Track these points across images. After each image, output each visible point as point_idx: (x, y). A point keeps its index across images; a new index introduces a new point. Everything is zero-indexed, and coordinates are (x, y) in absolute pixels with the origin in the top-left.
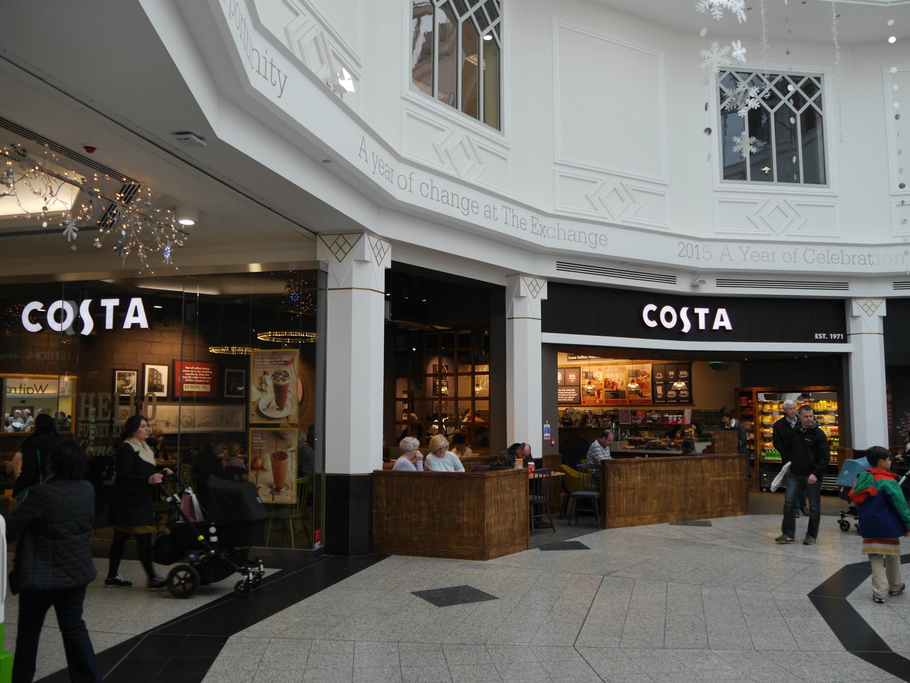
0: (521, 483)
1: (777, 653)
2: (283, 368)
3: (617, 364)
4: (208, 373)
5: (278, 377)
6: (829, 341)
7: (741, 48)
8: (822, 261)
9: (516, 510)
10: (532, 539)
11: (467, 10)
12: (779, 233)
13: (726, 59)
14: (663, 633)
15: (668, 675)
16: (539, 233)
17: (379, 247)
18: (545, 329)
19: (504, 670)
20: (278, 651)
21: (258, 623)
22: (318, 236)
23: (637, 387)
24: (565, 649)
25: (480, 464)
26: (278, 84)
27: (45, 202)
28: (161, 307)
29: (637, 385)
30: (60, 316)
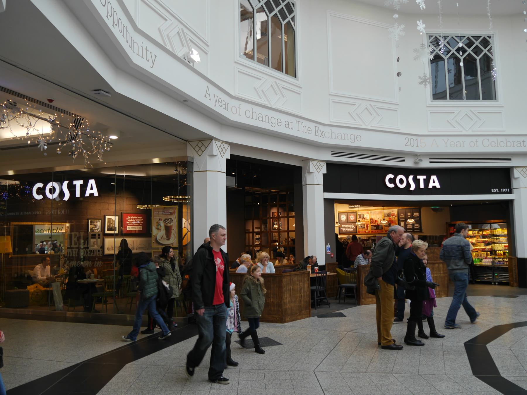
0: (305, 279)
1: (431, 376)
2: (169, 217)
3: (378, 209)
4: (141, 220)
5: (167, 222)
6: (500, 193)
7: (422, 24)
8: (493, 145)
9: (302, 295)
10: (313, 311)
11: (279, 11)
12: (467, 130)
13: (402, 32)
14: (368, 364)
15: (361, 387)
16: (320, 136)
17: (222, 147)
18: (325, 190)
19: (269, 384)
20: (149, 372)
21: (144, 357)
22: (188, 144)
23: (386, 222)
24: (308, 372)
25: (289, 269)
26: (151, 60)
27: (27, 130)
28: (112, 184)
29: (387, 221)
30: (52, 190)
